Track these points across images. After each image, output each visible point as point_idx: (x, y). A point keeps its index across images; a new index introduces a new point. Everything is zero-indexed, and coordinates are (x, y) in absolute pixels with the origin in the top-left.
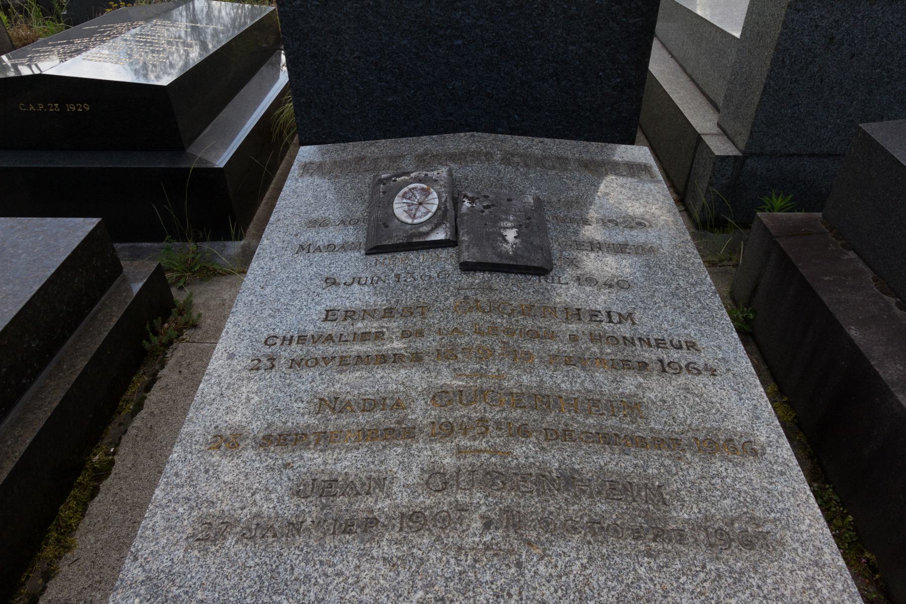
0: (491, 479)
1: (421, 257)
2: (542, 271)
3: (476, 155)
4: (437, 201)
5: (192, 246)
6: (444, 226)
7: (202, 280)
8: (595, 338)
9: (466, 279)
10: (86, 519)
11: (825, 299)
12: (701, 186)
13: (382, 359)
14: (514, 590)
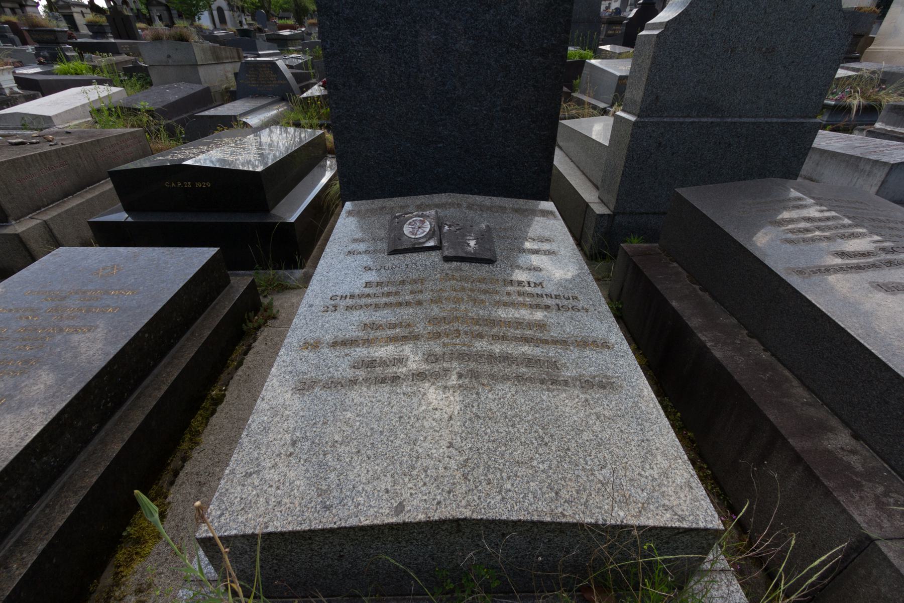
0: (461, 357)
2: (491, 261)
3: (452, 205)
5: (272, 272)
7: (278, 292)
8: (520, 294)
9: (447, 266)
10: (209, 427)
11: (659, 287)
12: (590, 232)
13: (400, 304)
14: (475, 404)
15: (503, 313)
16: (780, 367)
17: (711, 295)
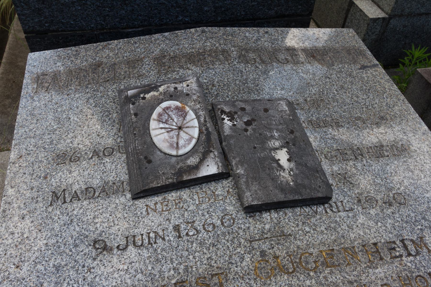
1: (196, 197)
4: (196, 123)
6: (212, 155)
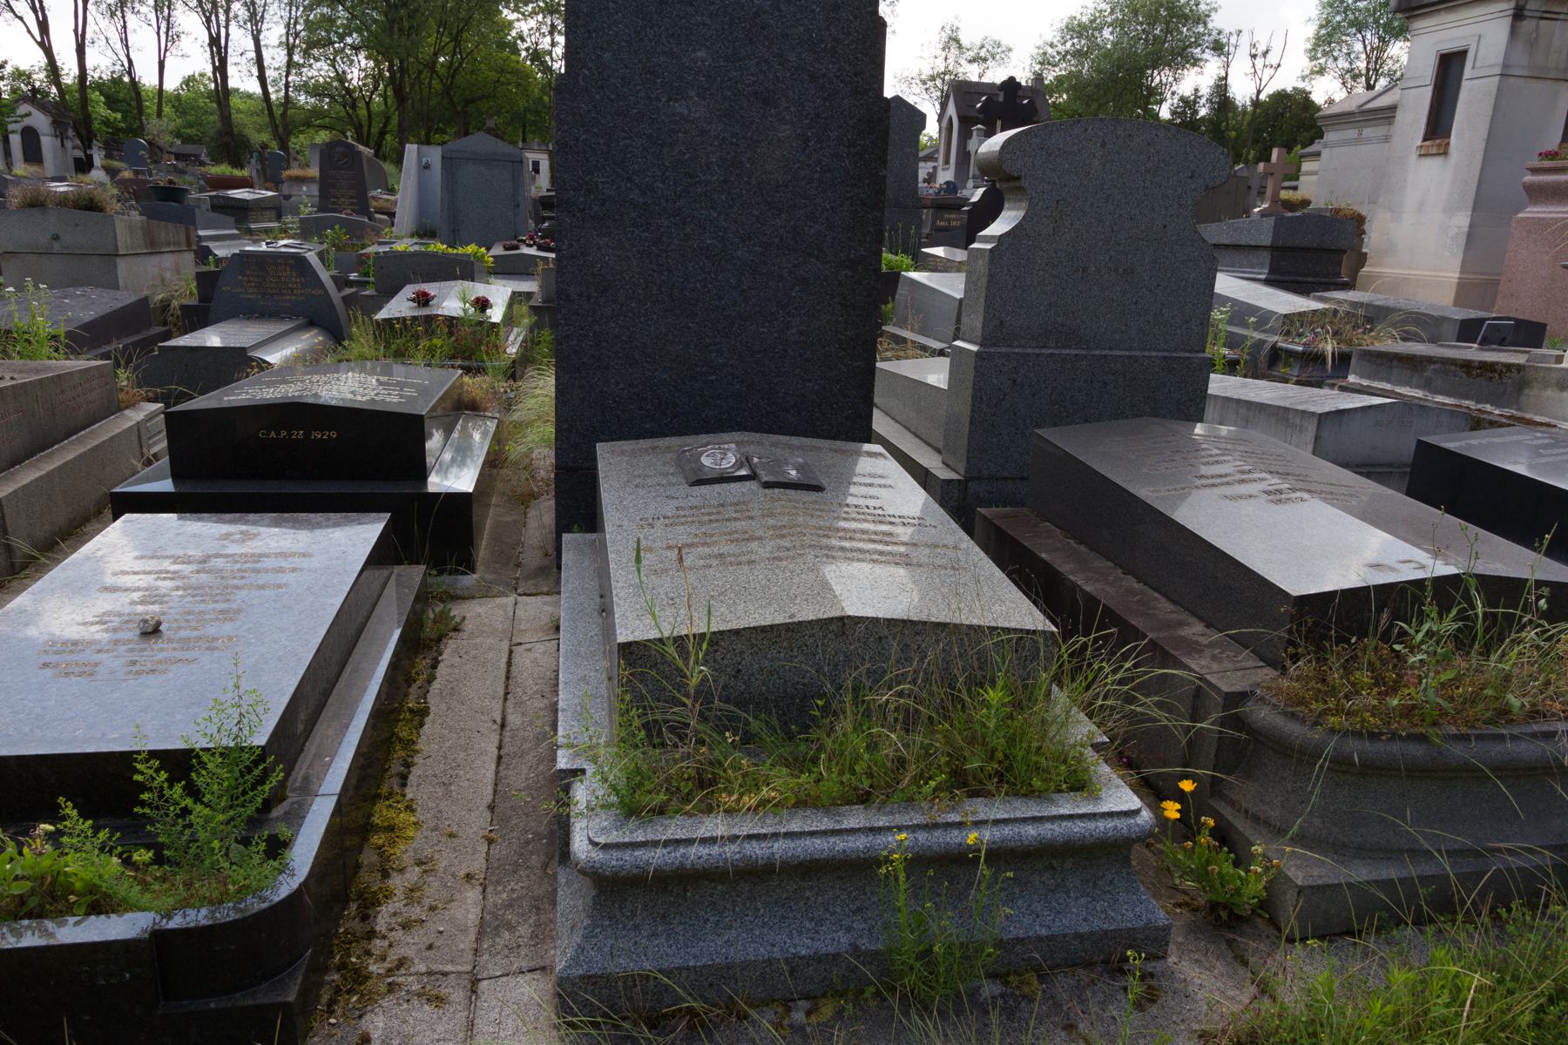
2: (818, 488)
15: (842, 524)
16: (1151, 592)
17: (1087, 545)
